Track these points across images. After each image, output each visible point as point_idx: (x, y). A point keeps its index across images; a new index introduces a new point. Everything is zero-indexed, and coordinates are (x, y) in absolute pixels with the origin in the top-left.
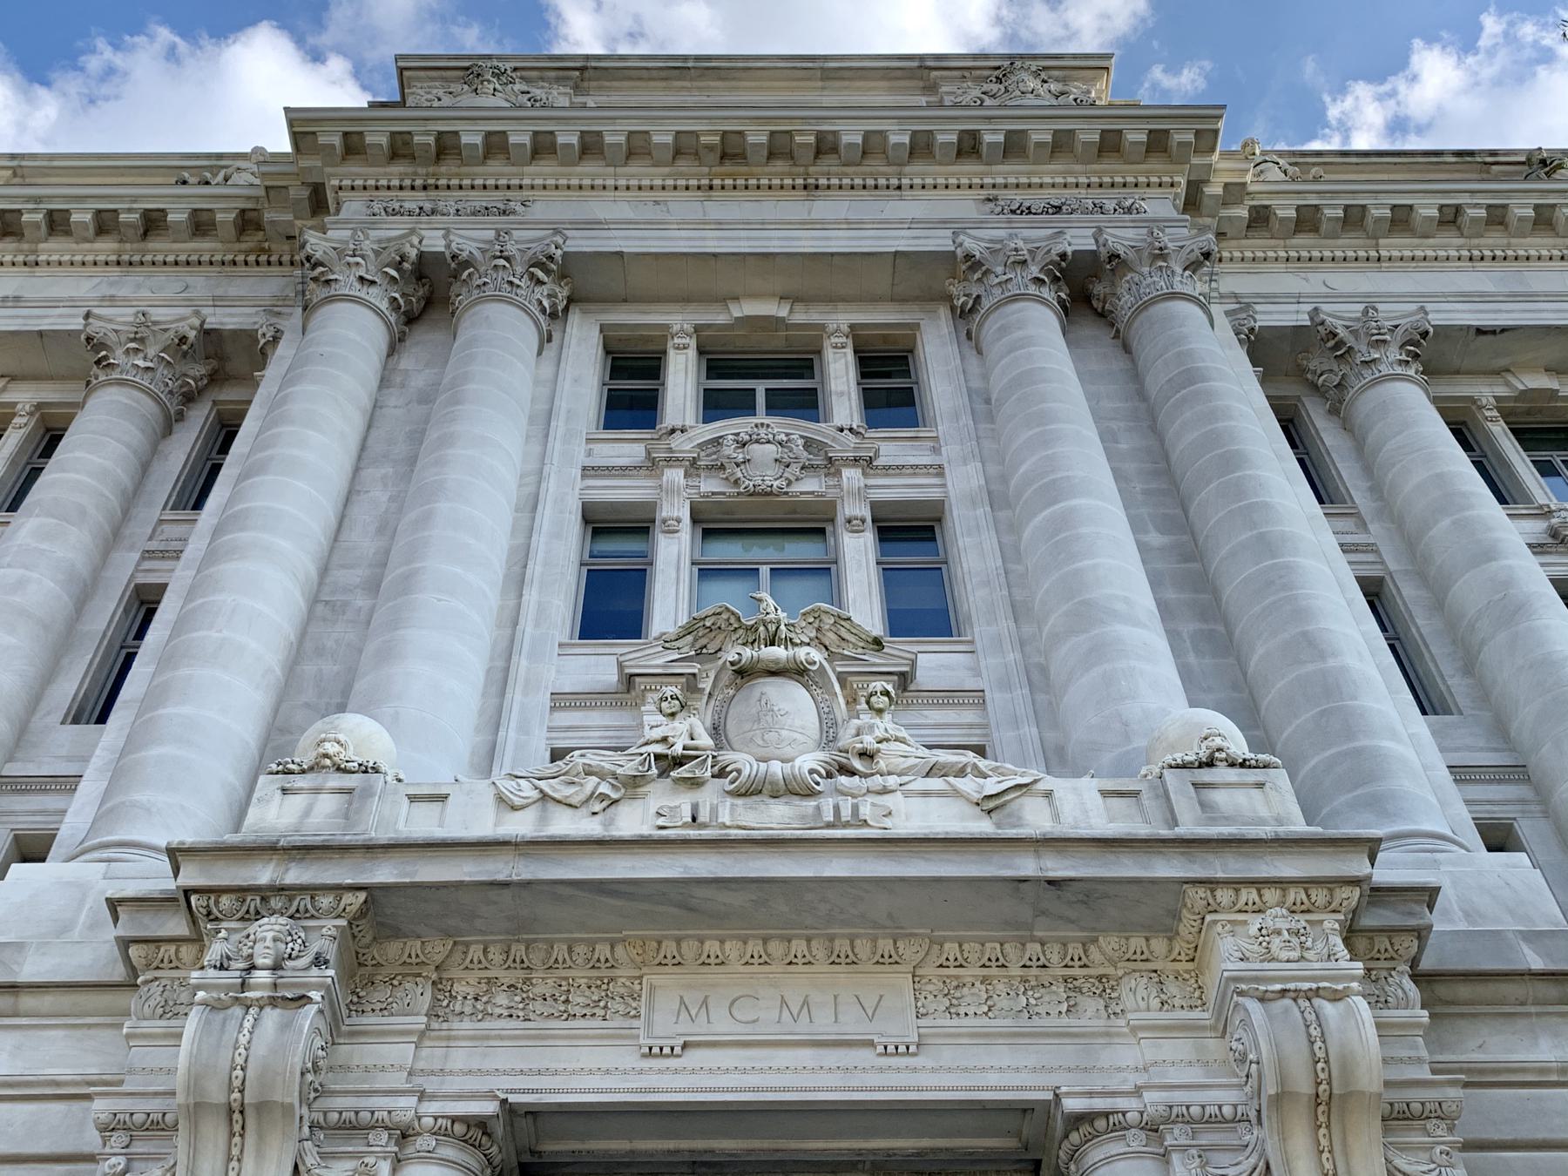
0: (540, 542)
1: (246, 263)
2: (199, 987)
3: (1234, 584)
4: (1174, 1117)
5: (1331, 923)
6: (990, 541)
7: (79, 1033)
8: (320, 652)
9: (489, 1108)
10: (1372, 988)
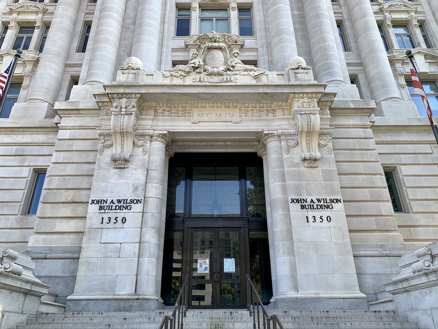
0: (167, 13)
2: (113, 111)
3: (311, 23)
4: (283, 134)
5: (315, 100)
6: (261, 13)
8: (125, 39)
9: (166, 132)
10: (321, 111)
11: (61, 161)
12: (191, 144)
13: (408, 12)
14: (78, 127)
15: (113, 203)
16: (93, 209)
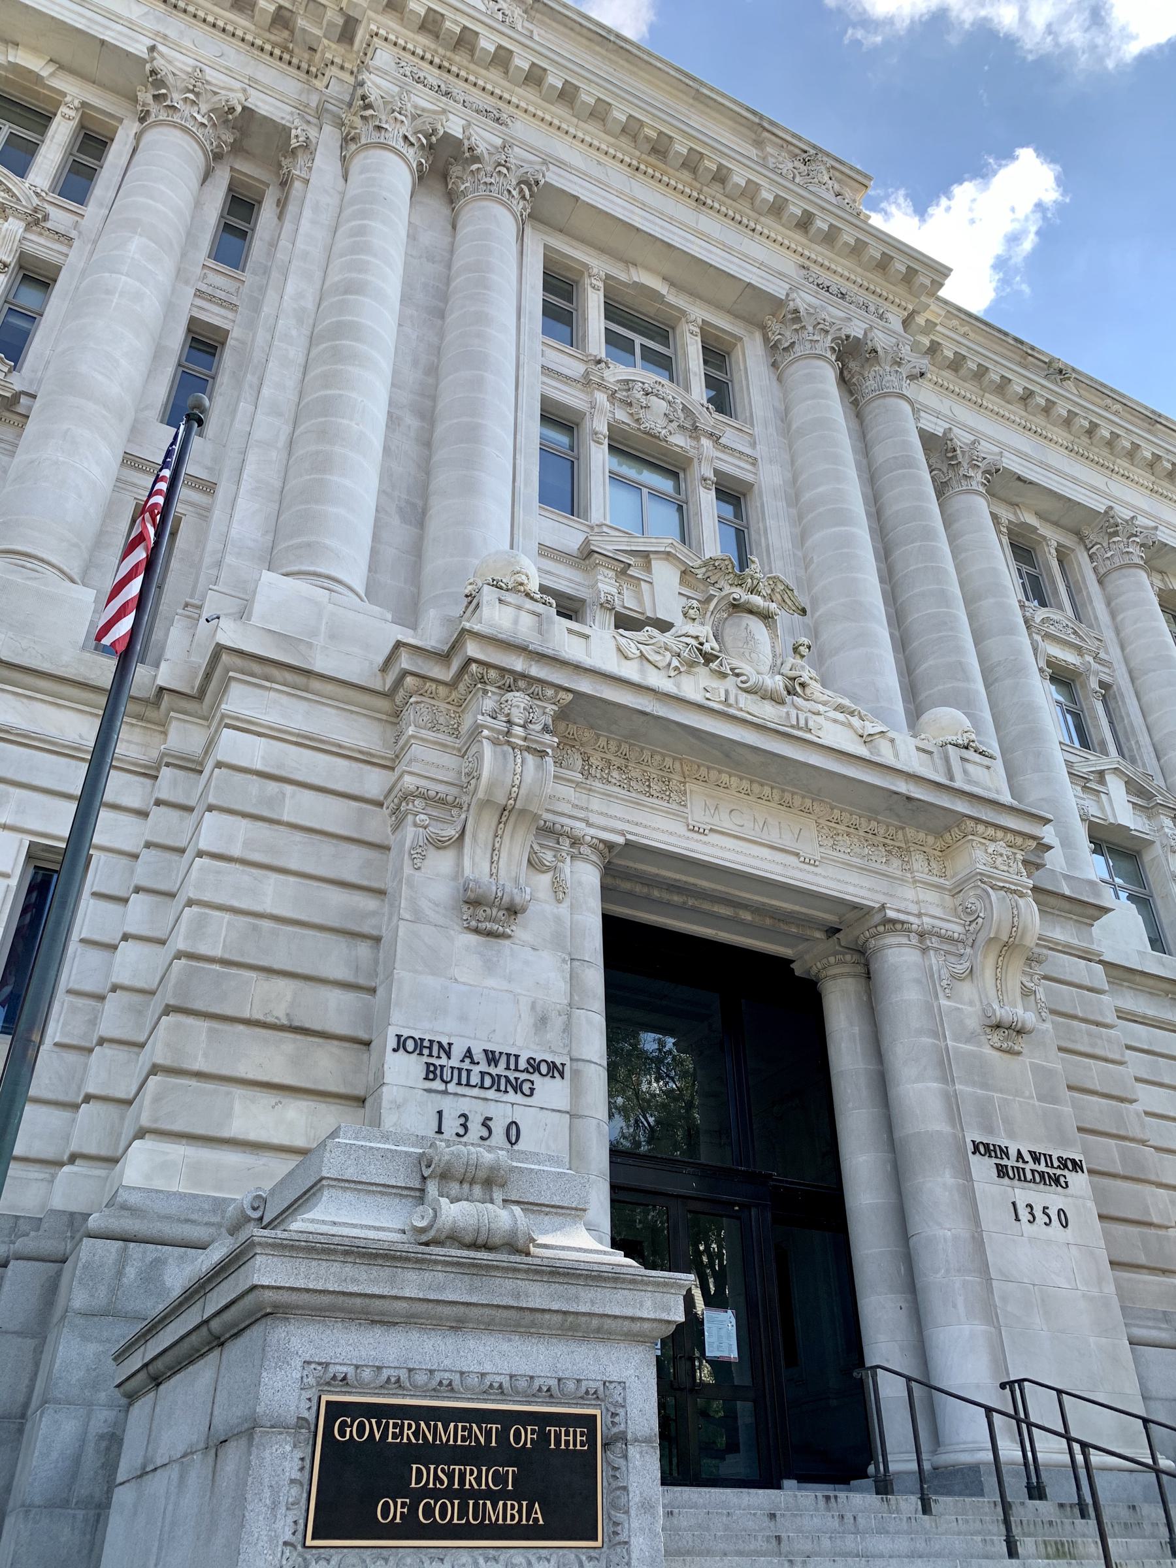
1: (271, 54)
7: (345, 714)
9: (621, 840)
11: (236, 852)
12: (638, 889)
13: (1079, 650)
14: (298, 735)
15: (473, 1062)
16: (402, 1072)
